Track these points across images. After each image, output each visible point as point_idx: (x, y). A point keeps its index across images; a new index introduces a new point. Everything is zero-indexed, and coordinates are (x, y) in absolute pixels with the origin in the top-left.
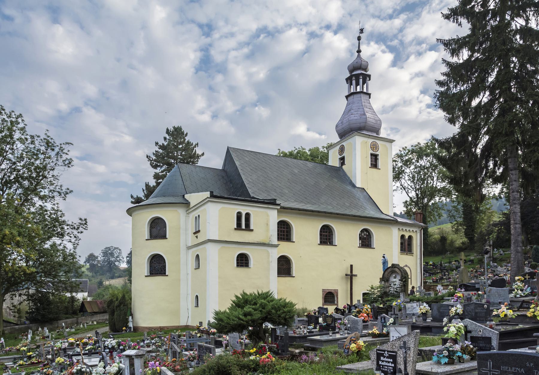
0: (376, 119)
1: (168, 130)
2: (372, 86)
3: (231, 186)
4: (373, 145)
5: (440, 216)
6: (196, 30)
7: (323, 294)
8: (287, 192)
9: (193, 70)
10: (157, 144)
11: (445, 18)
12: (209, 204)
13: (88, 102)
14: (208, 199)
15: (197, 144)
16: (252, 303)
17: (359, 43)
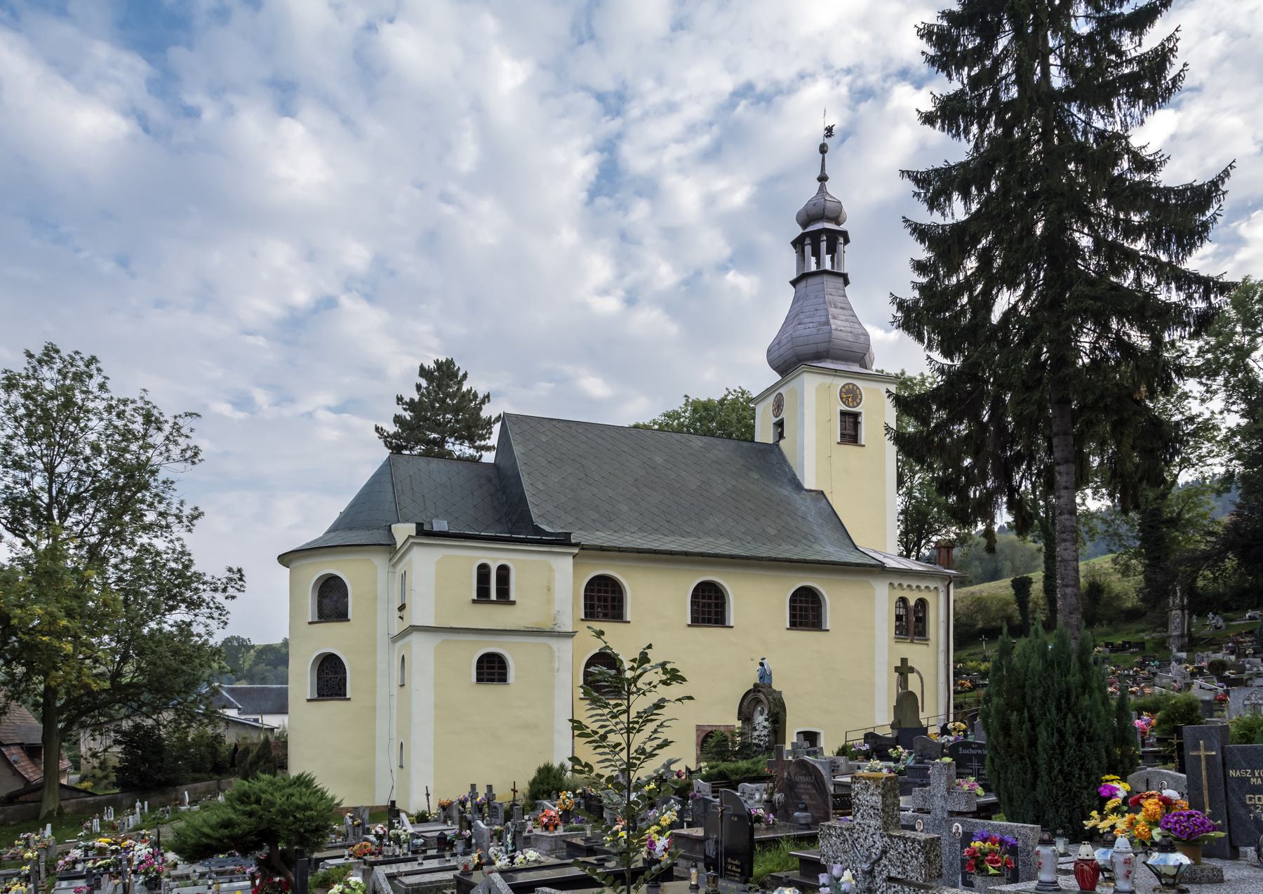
0: (856, 331)
1: (422, 368)
2: (850, 258)
6: (592, 105)
7: (698, 736)
9: (583, 196)
10: (400, 400)
11: (924, 122)
13: (350, 283)
14: (411, 540)
17: (823, 160)
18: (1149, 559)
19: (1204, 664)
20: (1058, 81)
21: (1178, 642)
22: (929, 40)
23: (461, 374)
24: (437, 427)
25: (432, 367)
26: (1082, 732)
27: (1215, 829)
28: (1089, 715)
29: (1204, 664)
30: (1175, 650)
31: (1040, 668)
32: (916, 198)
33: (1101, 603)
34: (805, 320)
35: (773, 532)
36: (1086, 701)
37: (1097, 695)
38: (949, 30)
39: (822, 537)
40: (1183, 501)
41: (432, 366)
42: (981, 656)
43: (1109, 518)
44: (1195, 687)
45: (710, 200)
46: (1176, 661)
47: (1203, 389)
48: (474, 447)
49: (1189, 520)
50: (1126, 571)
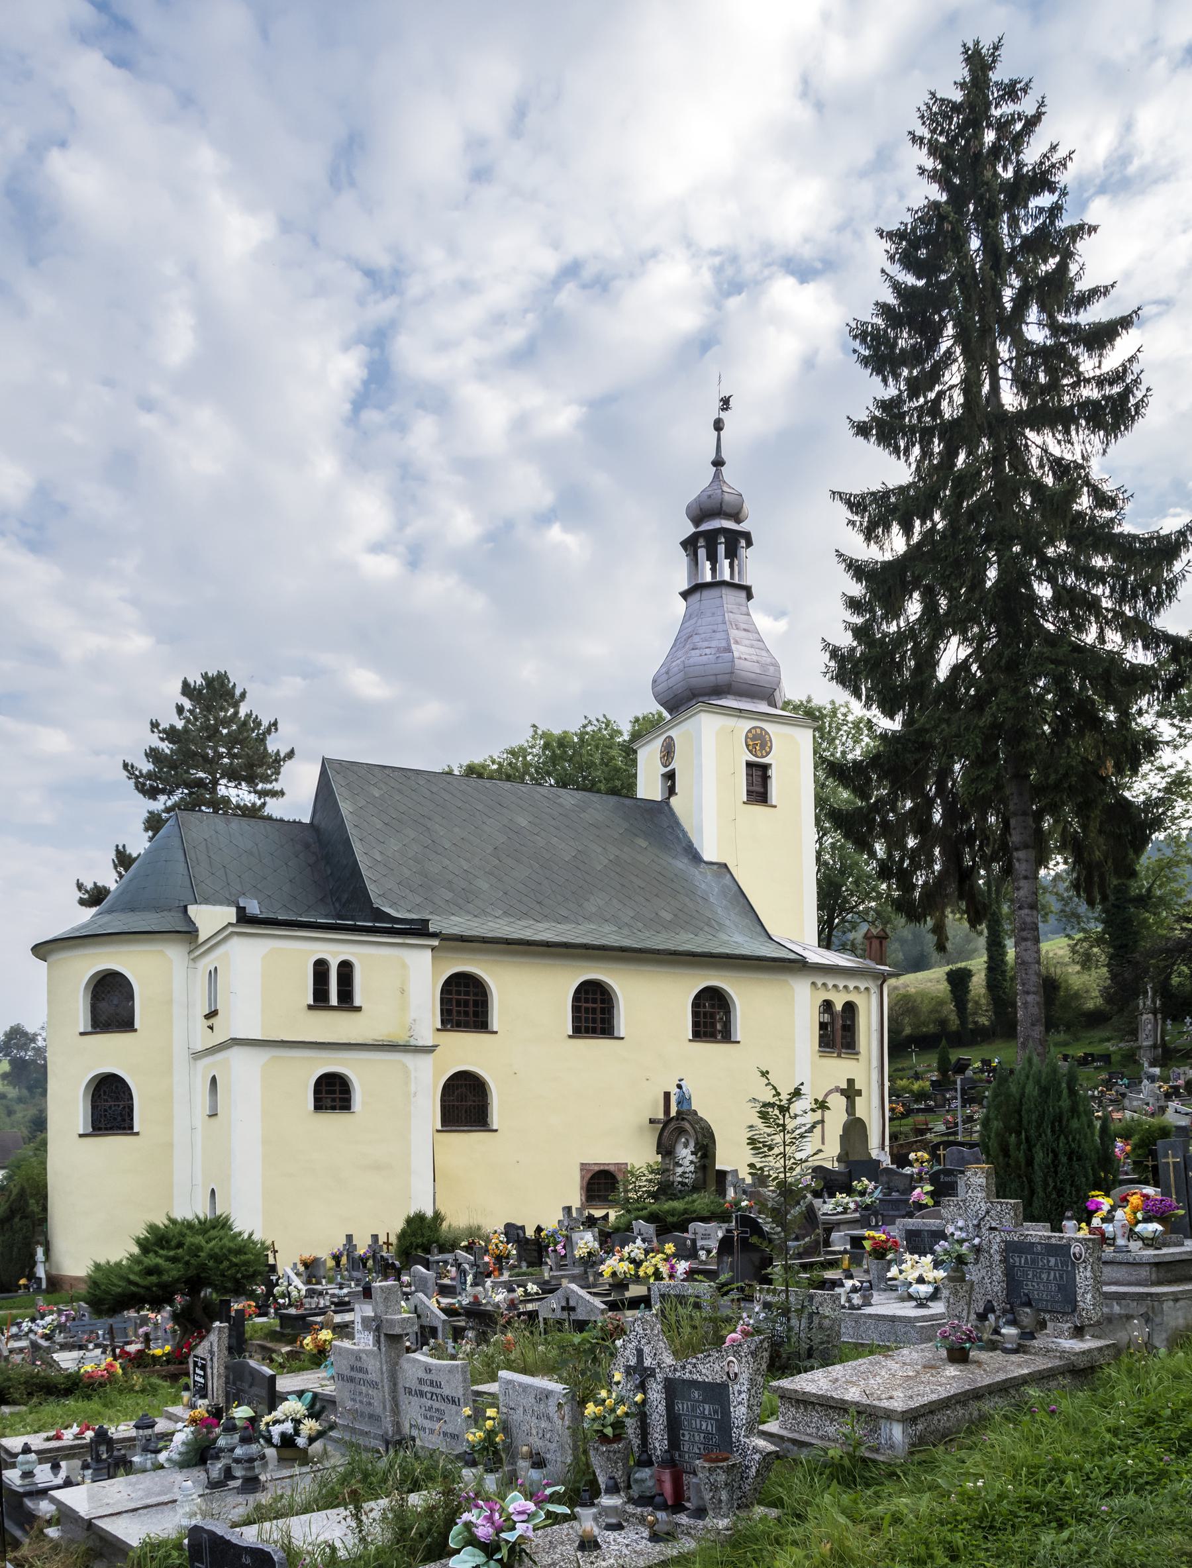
3: (329, 872)
4: (753, 739)
5: (1047, 914)
7: (582, 1177)
8: (485, 886)
9: (347, 407)
10: (154, 725)
12: (235, 942)
14: (231, 929)
15: (275, 724)
16: (173, 1243)
18: (1113, 947)
19: (1181, 1082)
20: (1010, 399)
21: (1150, 1055)
22: (863, 341)
23: (238, 692)
24: (209, 764)
25: (198, 683)
26: (1072, 1153)
27: (1178, 1208)
28: (1078, 1137)
29: (1181, 1082)
30: (1146, 1065)
31: (1036, 1093)
32: (850, 527)
33: (1057, 1002)
34: (700, 645)
35: (669, 917)
36: (1075, 1124)
37: (1084, 1119)
38: (885, 331)
39: (727, 923)
40: (1153, 873)
41: (200, 681)
42: (912, 1073)
43: (1066, 895)
44: (1170, 1111)
45: (521, 424)
46: (1148, 1078)
47: (1176, 732)
48: (256, 792)
49: (1160, 898)
50: (1086, 962)
